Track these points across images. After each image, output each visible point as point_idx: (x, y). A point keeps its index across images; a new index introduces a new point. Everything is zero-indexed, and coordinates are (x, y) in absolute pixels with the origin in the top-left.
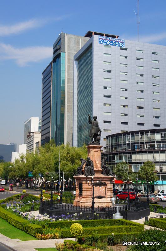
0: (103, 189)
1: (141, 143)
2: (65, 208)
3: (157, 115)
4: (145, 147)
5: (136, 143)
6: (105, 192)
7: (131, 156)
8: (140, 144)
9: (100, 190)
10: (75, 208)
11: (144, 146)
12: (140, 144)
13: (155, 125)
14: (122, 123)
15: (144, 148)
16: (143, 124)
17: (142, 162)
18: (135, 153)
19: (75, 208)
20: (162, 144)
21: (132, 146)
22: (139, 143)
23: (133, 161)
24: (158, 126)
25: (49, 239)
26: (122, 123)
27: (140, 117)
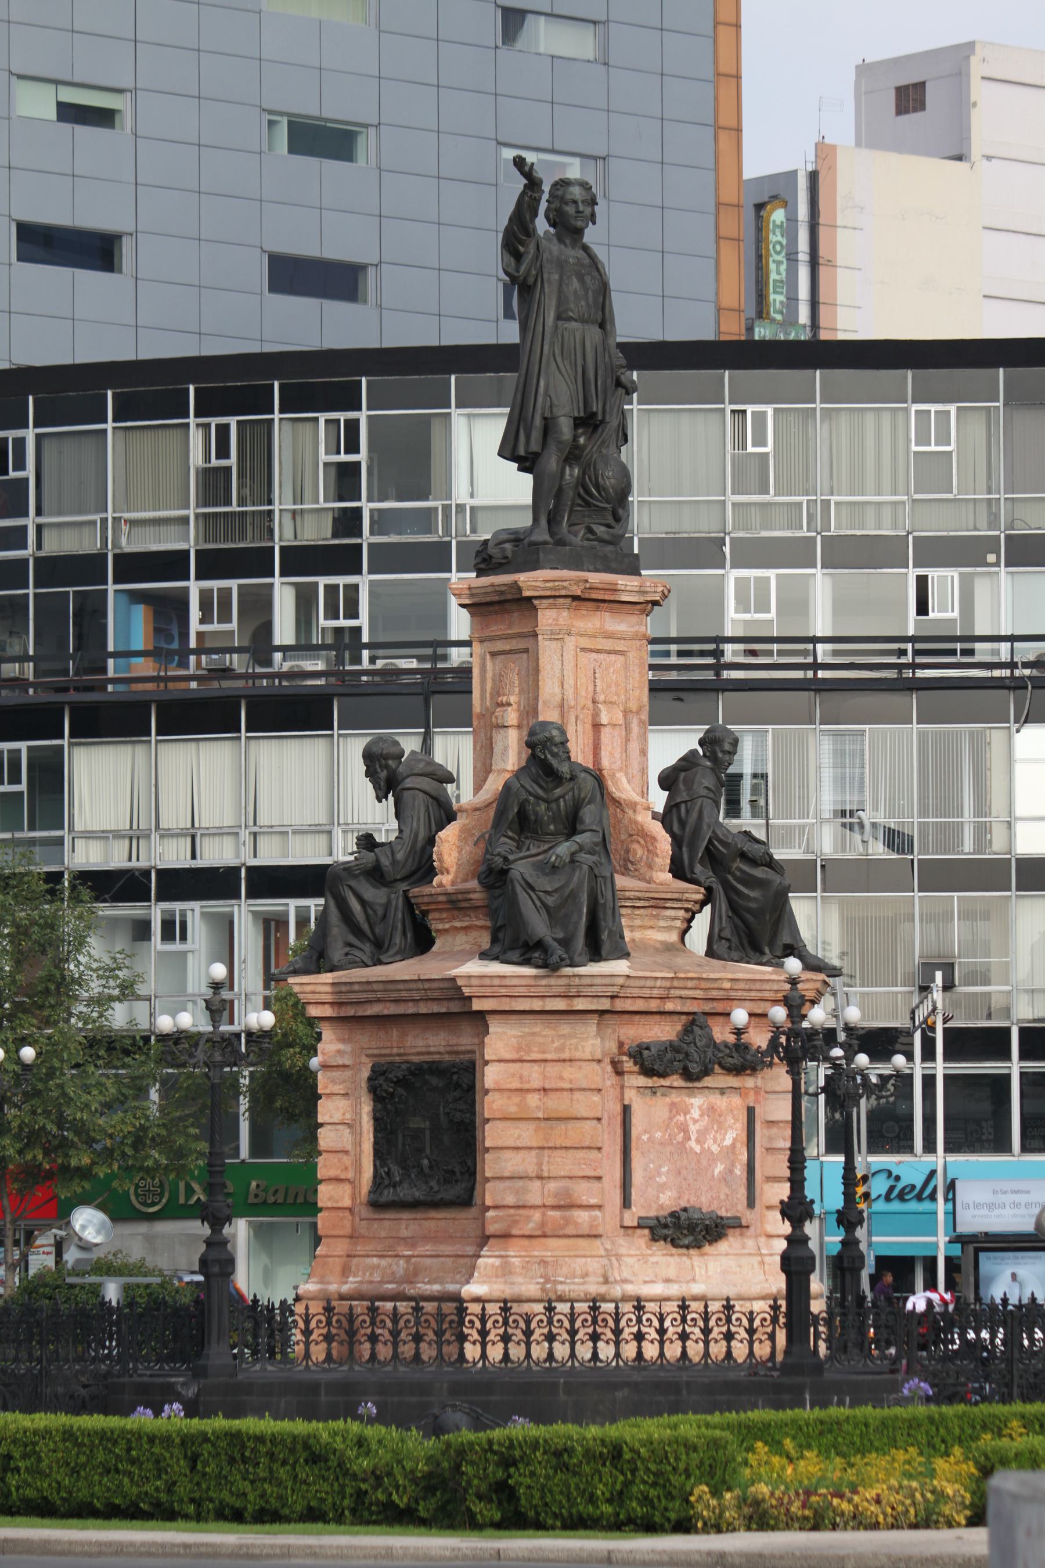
0: (721, 1127)
1: (212, 565)
2: (373, 1339)
3: (335, 108)
4: (284, 631)
5: (133, 566)
6: (740, 1171)
7: (50, 779)
8: (194, 587)
9: (692, 1144)
10: (550, 1338)
11: (258, 607)
12: (194, 587)
13: (291, 275)
14: (41, 243)
15: (260, 643)
16: (97, 251)
17: (232, 872)
18: (118, 721)
19: (595, 1337)
20: (206, 599)
21: (50, 612)
22: (172, 564)
23: (86, 856)
24: (334, 280)
25: (914, 1526)
26: (41, 243)
27: (70, 113)
